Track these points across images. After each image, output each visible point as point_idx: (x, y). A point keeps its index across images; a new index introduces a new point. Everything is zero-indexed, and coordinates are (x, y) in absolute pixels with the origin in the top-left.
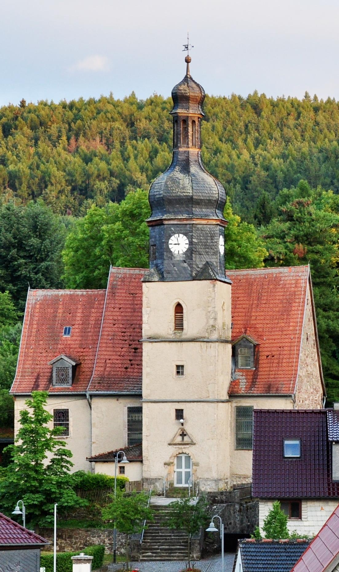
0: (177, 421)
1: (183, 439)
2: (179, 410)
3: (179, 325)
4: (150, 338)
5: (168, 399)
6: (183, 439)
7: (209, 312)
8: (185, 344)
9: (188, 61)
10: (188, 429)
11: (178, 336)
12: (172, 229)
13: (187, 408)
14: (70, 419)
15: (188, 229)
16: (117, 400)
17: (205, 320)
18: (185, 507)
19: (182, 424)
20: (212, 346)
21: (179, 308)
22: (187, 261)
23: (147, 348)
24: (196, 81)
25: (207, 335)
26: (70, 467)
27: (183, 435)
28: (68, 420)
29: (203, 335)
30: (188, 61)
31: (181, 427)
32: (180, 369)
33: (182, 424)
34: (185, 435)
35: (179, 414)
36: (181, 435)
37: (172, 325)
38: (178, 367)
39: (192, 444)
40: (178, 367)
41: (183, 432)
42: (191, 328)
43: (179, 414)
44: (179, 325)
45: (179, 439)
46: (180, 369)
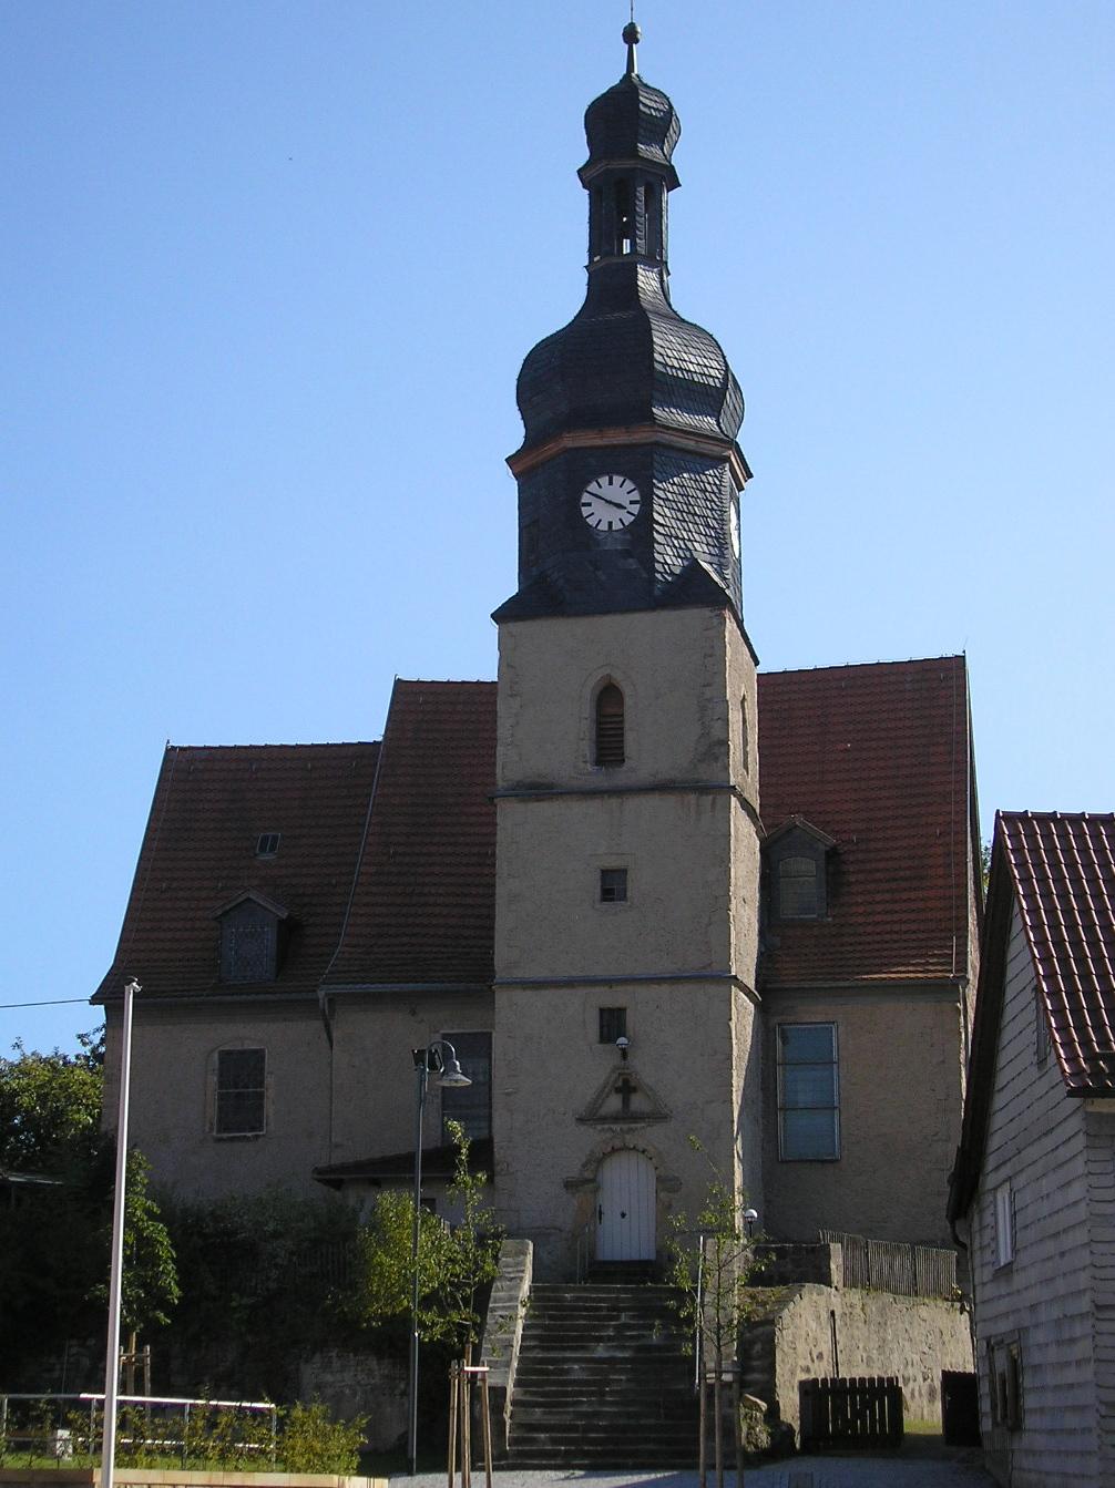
0: (608, 1047)
1: (626, 1102)
2: (611, 1010)
3: (609, 744)
6: (626, 1102)
8: (633, 803)
9: (630, 36)
10: (644, 1068)
11: (600, 779)
13: (640, 1004)
14: (269, 1080)
16: (414, 1013)
18: (517, 1370)
23: (844, 1373)
24: (690, 321)
27: (626, 1088)
28: (261, 1084)
32: (612, 886)
33: (624, 1054)
34: (634, 1090)
35: (612, 1024)
36: (618, 1090)
37: (587, 749)
38: (606, 874)
39: (658, 1117)
40: (606, 874)
43: (612, 1024)
45: (614, 1103)
46: (612, 886)
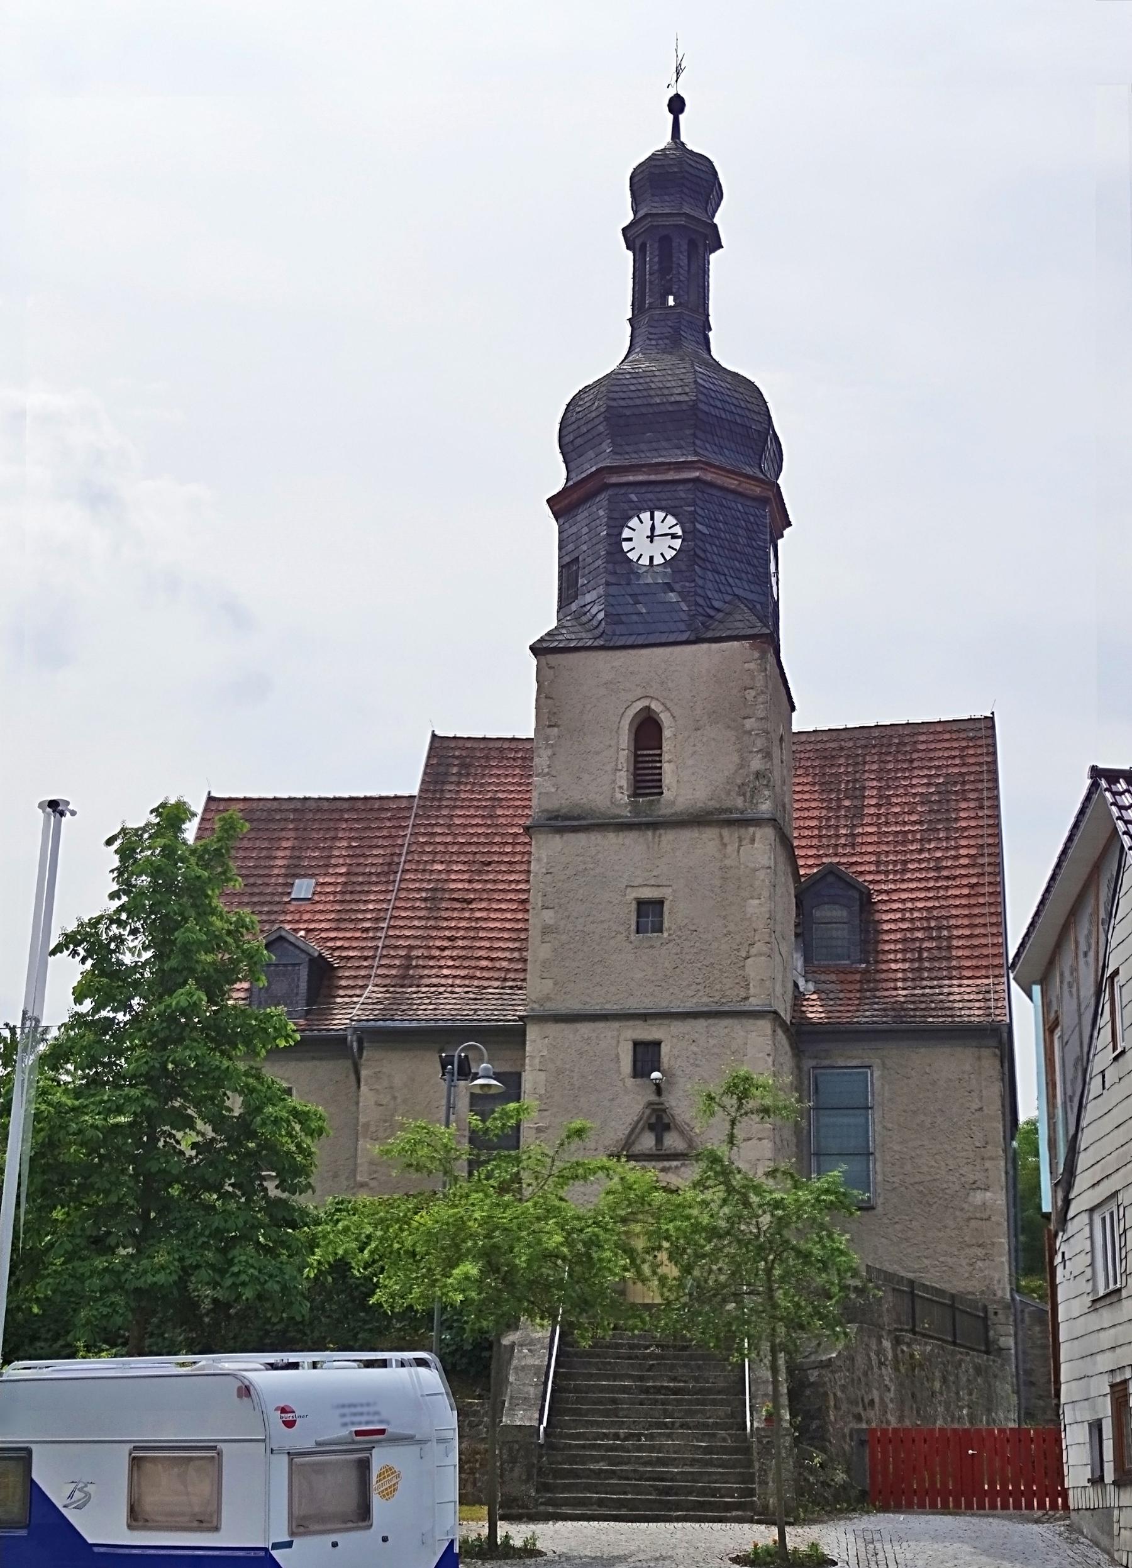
1: (659, 1141)
3: (646, 779)
4: (556, 818)
5: (611, 1007)
6: (659, 1141)
7: (749, 733)
12: (634, 497)
13: (674, 1041)
15: (683, 495)
17: (736, 758)
19: (658, 1089)
20: (758, 836)
21: (647, 731)
22: (677, 587)
25: (739, 802)
26: (524, 984)
29: (728, 804)
30: (677, 105)
31: (653, 1098)
32: (649, 913)
34: (667, 1128)
35: (646, 1056)
41: (659, 1118)
42: (684, 782)
43: (646, 1056)
44: (646, 779)
46: (649, 913)
